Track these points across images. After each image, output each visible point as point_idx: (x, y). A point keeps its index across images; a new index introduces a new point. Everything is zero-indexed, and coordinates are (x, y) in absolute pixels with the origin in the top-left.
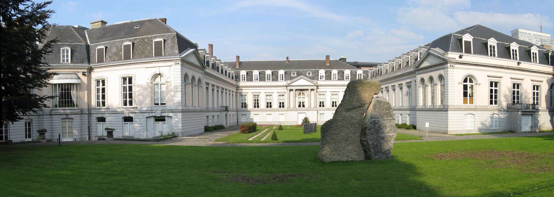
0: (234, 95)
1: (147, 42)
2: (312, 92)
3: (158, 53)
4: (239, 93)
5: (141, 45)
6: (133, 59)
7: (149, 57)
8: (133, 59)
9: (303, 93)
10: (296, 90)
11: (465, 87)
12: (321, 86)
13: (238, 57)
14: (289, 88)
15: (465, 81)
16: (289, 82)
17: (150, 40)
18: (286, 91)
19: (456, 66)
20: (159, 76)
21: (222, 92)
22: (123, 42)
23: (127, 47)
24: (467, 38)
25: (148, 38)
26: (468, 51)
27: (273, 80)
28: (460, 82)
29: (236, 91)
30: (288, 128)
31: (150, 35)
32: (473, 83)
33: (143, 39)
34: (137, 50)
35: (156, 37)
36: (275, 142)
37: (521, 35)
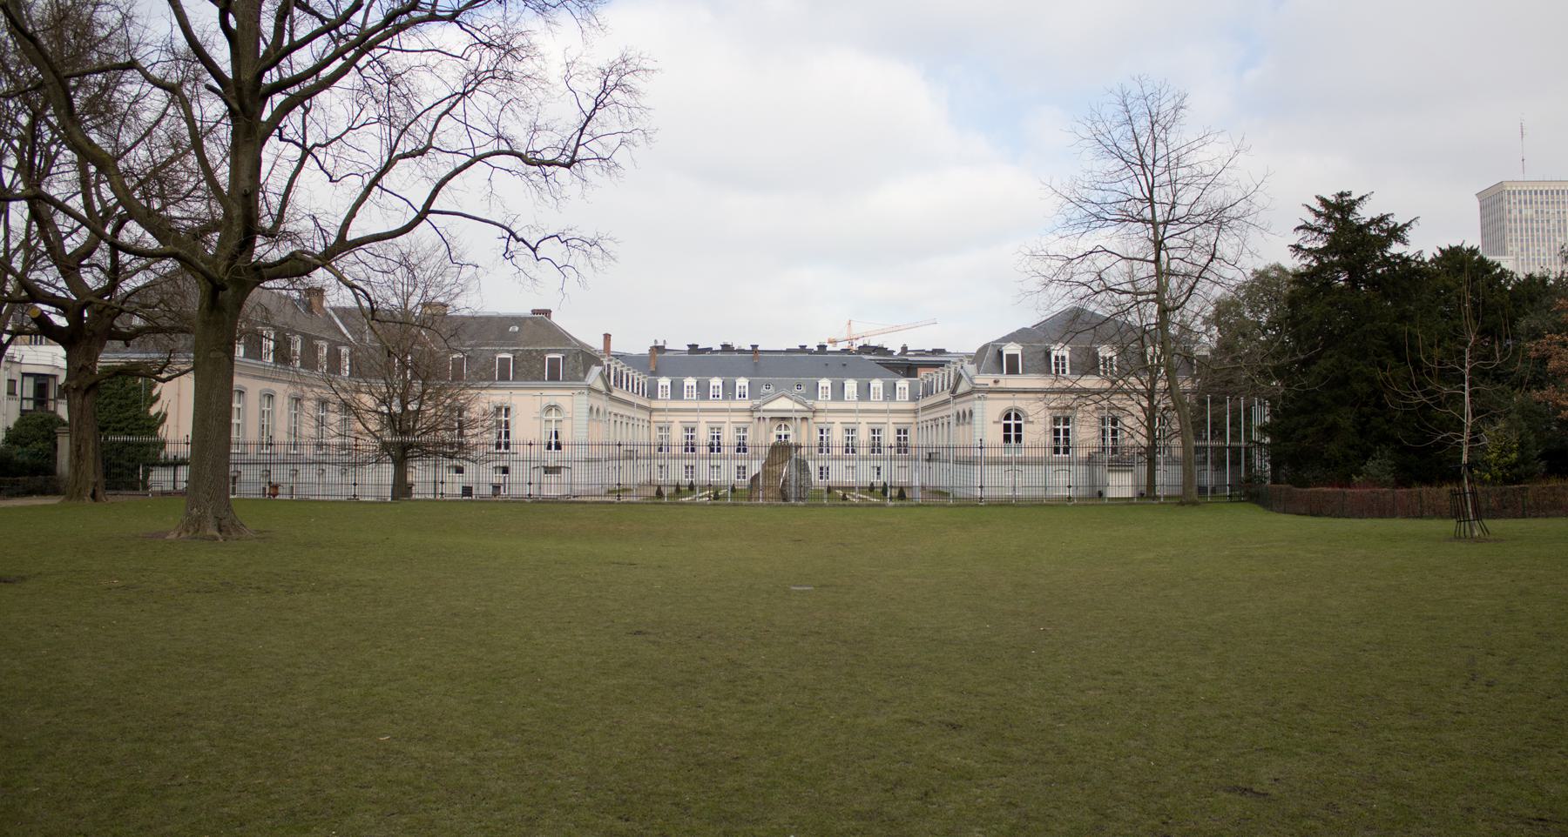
0: (646, 427)
1: (535, 358)
2: (805, 423)
3: (554, 376)
4: (654, 422)
5: (527, 361)
6: (513, 380)
7: (539, 379)
8: (513, 380)
9: (785, 425)
10: (772, 418)
11: (1007, 428)
12: (823, 411)
13: (656, 341)
14: (757, 415)
15: (1008, 417)
16: (757, 402)
17: (542, 354)
18: (749, 419)
19: (989, 396)
20: (554, 410)
21: (627, 424)
22: (496, 352)
23: (504, 362)
24: (1012, 349)
25: (537, 351)
26: (1013, 370)
27: (725, 397)
28: (997, 419)
29: (648, 418)
30: (28, 158)
31: (541, 346)
32: (1021, 420)
33: (530, 352)
34: (520, 368)
35: (549, 351)
36: (640, 407)
37: (1537, 212)
